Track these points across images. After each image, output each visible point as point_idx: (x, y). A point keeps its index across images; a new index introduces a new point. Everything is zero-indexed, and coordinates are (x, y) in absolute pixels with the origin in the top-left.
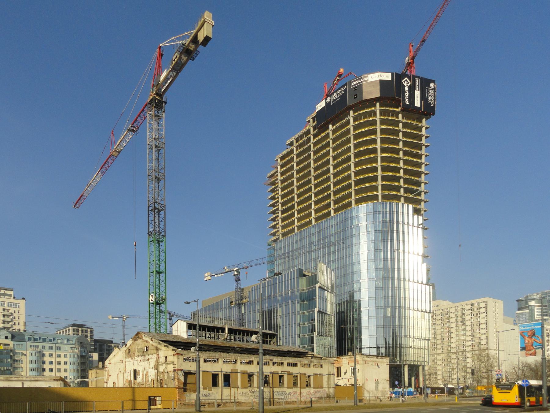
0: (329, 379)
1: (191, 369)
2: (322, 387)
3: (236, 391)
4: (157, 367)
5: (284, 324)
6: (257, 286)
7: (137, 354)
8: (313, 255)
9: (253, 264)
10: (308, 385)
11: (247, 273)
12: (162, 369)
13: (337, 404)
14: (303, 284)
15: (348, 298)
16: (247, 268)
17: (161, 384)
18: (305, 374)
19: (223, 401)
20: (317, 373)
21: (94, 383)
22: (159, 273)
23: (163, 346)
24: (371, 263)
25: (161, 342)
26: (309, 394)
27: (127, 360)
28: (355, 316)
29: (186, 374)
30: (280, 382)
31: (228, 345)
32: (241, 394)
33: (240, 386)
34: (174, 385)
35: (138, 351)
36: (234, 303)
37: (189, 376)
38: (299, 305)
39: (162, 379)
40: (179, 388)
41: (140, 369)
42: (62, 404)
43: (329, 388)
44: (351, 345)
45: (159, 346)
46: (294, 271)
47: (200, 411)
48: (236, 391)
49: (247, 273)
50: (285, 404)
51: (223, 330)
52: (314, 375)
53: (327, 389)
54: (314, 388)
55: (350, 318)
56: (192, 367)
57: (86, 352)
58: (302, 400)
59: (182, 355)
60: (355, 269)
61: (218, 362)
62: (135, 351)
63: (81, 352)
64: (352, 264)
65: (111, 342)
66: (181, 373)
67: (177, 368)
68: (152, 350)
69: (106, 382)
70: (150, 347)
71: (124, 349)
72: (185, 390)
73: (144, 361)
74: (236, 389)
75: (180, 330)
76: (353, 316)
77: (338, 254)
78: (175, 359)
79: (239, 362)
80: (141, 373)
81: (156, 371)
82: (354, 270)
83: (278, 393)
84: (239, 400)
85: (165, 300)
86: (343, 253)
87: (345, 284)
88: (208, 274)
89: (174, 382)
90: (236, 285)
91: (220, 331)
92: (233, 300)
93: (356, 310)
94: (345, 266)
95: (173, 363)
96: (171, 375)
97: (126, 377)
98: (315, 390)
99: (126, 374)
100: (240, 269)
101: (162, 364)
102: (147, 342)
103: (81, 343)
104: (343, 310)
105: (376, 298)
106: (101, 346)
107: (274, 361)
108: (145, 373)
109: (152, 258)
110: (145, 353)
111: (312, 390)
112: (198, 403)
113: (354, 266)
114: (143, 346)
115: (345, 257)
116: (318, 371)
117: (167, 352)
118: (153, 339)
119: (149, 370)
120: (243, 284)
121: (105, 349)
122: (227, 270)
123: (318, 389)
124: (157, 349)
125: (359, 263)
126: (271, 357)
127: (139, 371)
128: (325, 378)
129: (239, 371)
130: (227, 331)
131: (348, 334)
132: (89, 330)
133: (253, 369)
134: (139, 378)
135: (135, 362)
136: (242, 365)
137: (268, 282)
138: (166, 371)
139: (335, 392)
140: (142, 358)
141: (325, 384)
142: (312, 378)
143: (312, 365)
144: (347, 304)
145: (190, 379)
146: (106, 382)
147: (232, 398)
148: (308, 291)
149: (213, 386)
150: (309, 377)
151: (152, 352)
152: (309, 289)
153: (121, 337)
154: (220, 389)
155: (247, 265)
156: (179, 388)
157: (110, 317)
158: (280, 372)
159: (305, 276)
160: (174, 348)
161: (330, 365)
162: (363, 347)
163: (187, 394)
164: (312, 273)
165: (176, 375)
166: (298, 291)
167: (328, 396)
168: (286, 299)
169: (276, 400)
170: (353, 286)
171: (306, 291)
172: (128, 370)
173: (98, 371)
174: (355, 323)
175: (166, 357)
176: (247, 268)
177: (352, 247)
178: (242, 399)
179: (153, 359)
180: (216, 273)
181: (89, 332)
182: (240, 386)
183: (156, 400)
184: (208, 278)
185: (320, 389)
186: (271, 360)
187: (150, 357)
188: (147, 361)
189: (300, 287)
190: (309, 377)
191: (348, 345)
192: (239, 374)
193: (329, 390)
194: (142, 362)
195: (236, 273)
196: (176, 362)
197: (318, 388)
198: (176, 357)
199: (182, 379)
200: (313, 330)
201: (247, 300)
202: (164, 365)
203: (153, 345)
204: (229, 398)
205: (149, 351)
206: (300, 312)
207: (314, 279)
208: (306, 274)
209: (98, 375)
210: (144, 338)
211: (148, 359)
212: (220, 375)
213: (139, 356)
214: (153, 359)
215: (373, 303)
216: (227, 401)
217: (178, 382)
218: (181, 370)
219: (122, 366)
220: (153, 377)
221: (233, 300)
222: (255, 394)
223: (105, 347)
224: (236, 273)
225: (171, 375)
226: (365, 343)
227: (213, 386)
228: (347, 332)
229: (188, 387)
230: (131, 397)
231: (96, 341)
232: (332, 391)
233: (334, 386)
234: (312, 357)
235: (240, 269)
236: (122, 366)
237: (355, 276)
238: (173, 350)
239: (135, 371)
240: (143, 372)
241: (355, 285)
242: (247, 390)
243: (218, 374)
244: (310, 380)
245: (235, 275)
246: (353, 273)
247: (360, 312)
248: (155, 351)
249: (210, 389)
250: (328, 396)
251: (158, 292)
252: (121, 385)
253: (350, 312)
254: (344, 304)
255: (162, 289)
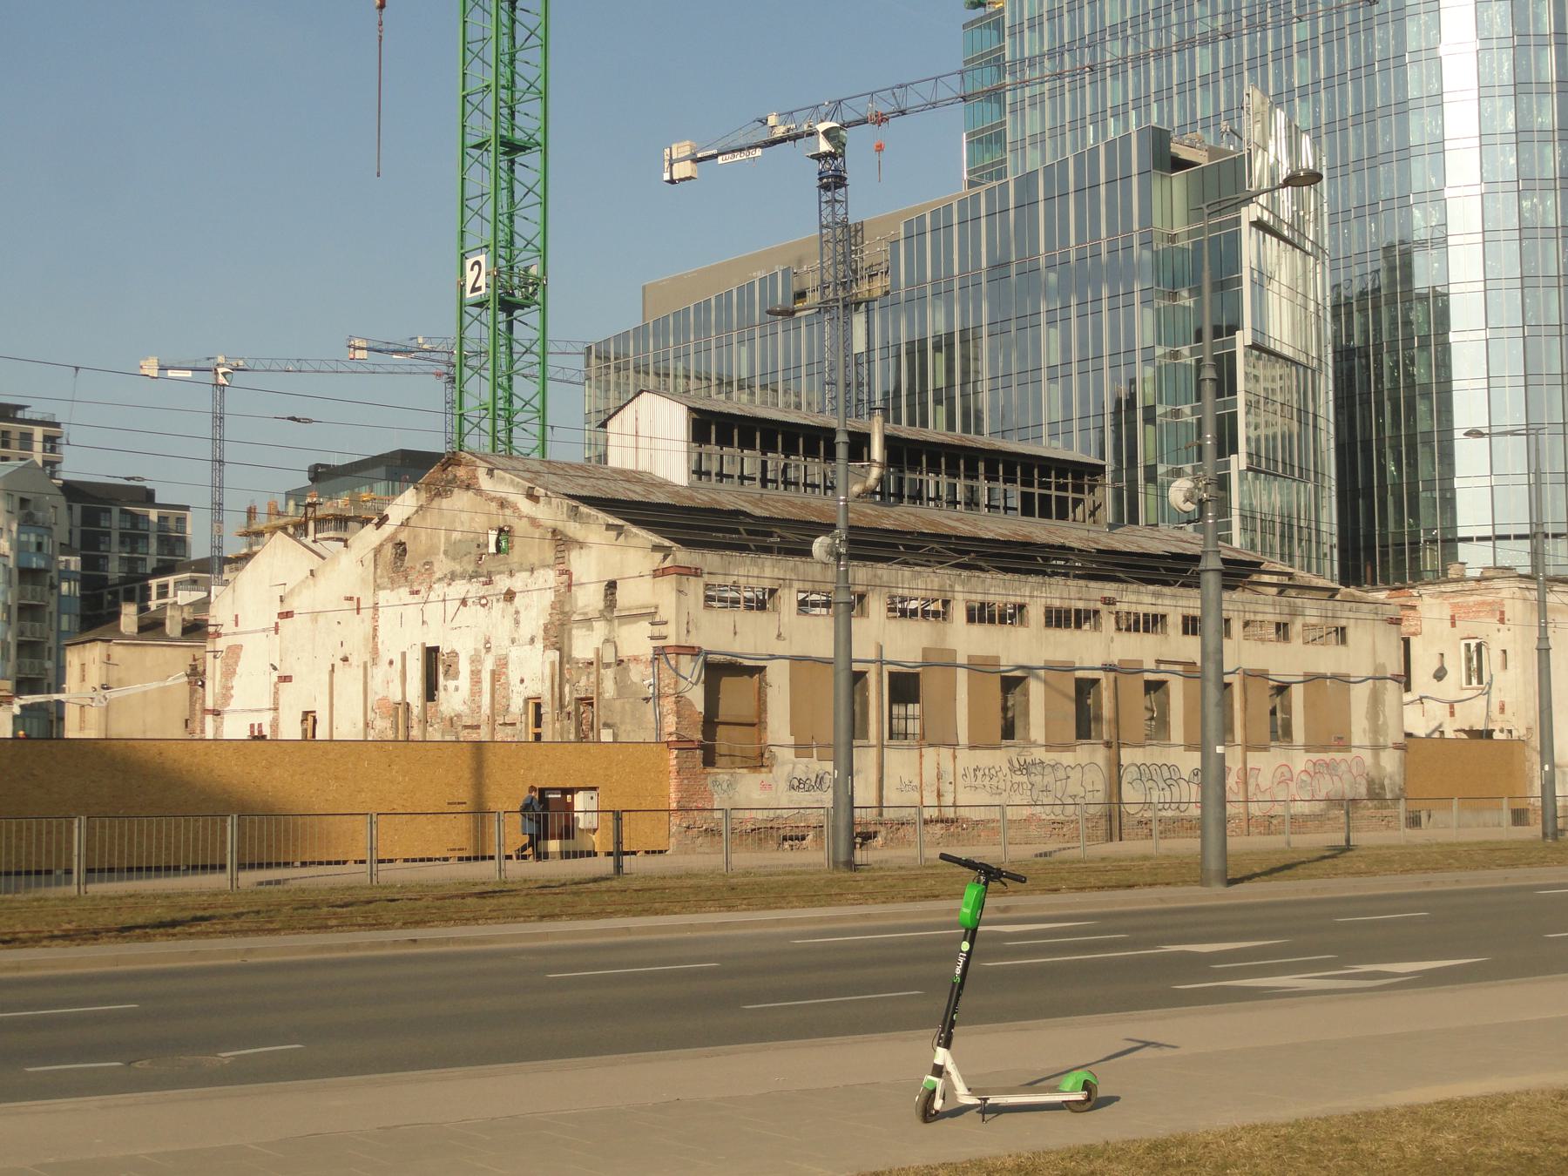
0: (1376, 701)
1: (736, 649)
2: (1343, 744)
3: (947, 765)
4: (557, 634)
5: (1076, 414)
6: (935, 213)
7: (442, 565)
8: (1203, 60)
9: (912, 101)
10: (1281, 732)
11: (880, 148)
12: (584, 645)
13: (1417, 836)
14: (1172, 201)
15: (1383, 278)
16: (881, 119)
17: (579, 724)
18: (1263, 675)
19: (887, 814)
20: (1322, 670)
21: (93, 714)
22: (512, 148)
23: (594, 530)
24: (1499, 103)
25: (584, 509)
26: (1286, 780)
27: (384, 596)
28: (1419, 372)
29: (718, 671)
30: (538, 706)
31: (888, 524)
32: (970, 780)
33: (963, 738)
34: (659, 729)
35: (453, 552)
36: (813, 298)
37: (727, 684)
38: (1149, 314)
39: (587, 701)
40: (682, 744)
41: (459, 642)
42: (231, 823)
43: (1376, 748)
44: (1400, 522)
45: (573, 529)
46: (1126, 139)
47: (851, 865)
48: (947, 765)
49: (880, 148)
50: (1164, 834)
51: (859, 445)
52: (1311, 679)
53: (1367, 756)
54: (1308, 748)
55: (1395, 380)
56: (730, 634)
57: (48, 548)
58: (1255, 809)
59: (697, 573)
60: (1418, 129)
61: (1023, 622)
62: (432, 550)
63: (20, 548)
64: (1403, 108)
65: (148, 497)
66: (690, 668)
67: (672, 641)
68: (530, 546)
69: (217, 713)
70: (520, 526)
71: (368, 537)
72: (709, 760)
73: (483, 602)
74: (946, 753)
75: (653, 441)
76: (1409, 375)
77: (1329, 54)
78: (664, 594)
79: (959, 612)
80: (464, 667)
81: (554, 655)
82: (1414, 139)
83: (1145, 774)
84: (964, 813)
85: (539, 283)
86: (1356, 52)
87: (1369, 209)
88: (681, 149)
89: (652, 716)
90: (827, 210)
91: (981, 466)
92: (811, 281)
93: (1424, 345)
94: (1367, 116)
95: (650, 615)
96: (640, 675)
97: (376, 684)
98: (1315, 756)
99: (379, 674)
100: (844, 126)
101: (587, 621)
102: (503, 504)
103: (24, 502)
104: (1357, 341)
105: (1526, 281)
106: (90, 518)
107: (1122, 607)
108: (488, 665)
109: (482, 75)
110: (488, 564)
111: (1300, 761)
112: (842, 823)
113: (1414, 120)
114: (480, 522)
115: (1364, 70)
116: (1327, 659)
117: (631, 559)
118: (540, 491)
119: (514, 653)
120: (865, 202)
121: (115, 536)
122: (780, 132)
123: (1326, 757)
124: (562, 542)
125: (1436, 101)
126: (1110, 589)
127: (455, 654)
128: (1360, 695)
129: (962, 659)
130: (877, 451)
131: (1382, 469)
132: (38, 433)
133: (1020, 646)
134: (455, 696)
135: (434, 611)
136: (978, 630)
137: (990, 192)
138: (609, 657)
139: (1405, 765)
140: (474, 589)
141: (1359, 731)
142: (1297, 693)
143: (1296, 628)
144: (1376, 308)
145: (735, 696)
146: (217, 713)
147: (930, 799)
148: (1198, 246)
149: (1079, 737)
150: (1282, 689)
151: (533, 558)
152: (1200, 231)
153: (204, 472)
154: (873, 753)
155: (884, 108)
156: (682, 744)
157: (150, 367)
158: (1149, 664)
159: (1179, 164)
160: (657, 539)
161: (1381, 628)
162: (1461, 533)
163: (721, 775)
164: (1213, 152)
165: (667, 677)
166: (1146, 243)
167: (1376, 793)
168: (1082, 277)
169: (1132, 810)
170: (1410, 216)
171: (1183, 243)
172: (391, 646)
173: (118, 652)
174: (1421, 407)
175: (612, 586)
176: (881, 119)
177: (1400, 21)
178: (971, 800)
179: (536, 595)
180: (722, 145)
181: (38, 446)
182: (963, 738)
183: (570, 807)
184: (683, 170)
185: (1338, 756)
186: (1109, 602)
187: (518, 582)
188: (499, 607)
189: (1157, 222)
190: (1282, 689)
191: (1383, 523)
192: (962, 676)
193: (1376, 757)
194: (473, 610)
195: (825, 146)
196: (667, 611)
197: (1325, 748)
198: (667, 585)
199: (697, 697)
200: (1226, 444)
201: (878, 285)
202: (600, 628)
203: (534, 522)
204: (915, 797)
205: (515, 557)
206: (1159, 351)
207: (1224, 186)
208: (1185, 154)
209: (115, 673)
210: (485, 482)
211: (510, 596)
212: (872, 678)
213: (453, 577)
214: (536, 595)
215: (1509, 306)
216: (905, 814)
217: (679, 714)
218: (693, 651)
219: (357, 628)
220: (539, 686)
221: (811, 281)
222: (1037, 779)
223: (114, 521)
224: (825, 146)
225: (640, 675)
226: (1472, 514)
227: (1079, 737)
228: (1381, 455)
229: (725, 739)
230: (464, 793)
231: (73, 491)
232: (1390, 762)
233: (1401, 739)
234: (1282, 589)
235: (844, 126)
236: (357, 628)
237: (1417, 166)
238: (656, 548)
239: (431, 655)
240: (475, 660)
241: (1417, 213)
242: (997, 758)
243: (891, 674)
244: (1287, 709)
245: (819, 157)
246: (1405, 153)
247: (1445, 348)
248: (550, 555)
249: (1066, 747)
250: (1376, 793)
251: (505, 246)
252: (348, 727)
253: (1393, 351)
254: (1363, 310)
255: (526, 228)
